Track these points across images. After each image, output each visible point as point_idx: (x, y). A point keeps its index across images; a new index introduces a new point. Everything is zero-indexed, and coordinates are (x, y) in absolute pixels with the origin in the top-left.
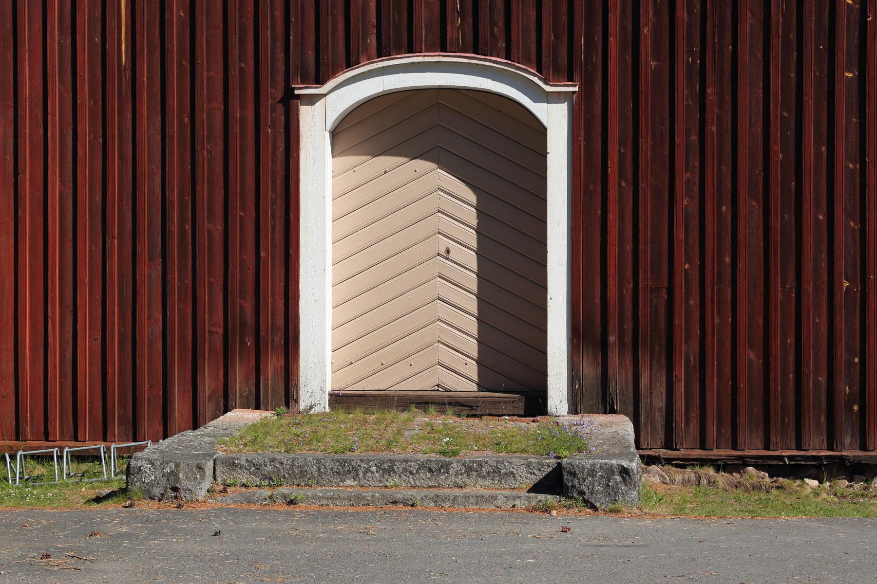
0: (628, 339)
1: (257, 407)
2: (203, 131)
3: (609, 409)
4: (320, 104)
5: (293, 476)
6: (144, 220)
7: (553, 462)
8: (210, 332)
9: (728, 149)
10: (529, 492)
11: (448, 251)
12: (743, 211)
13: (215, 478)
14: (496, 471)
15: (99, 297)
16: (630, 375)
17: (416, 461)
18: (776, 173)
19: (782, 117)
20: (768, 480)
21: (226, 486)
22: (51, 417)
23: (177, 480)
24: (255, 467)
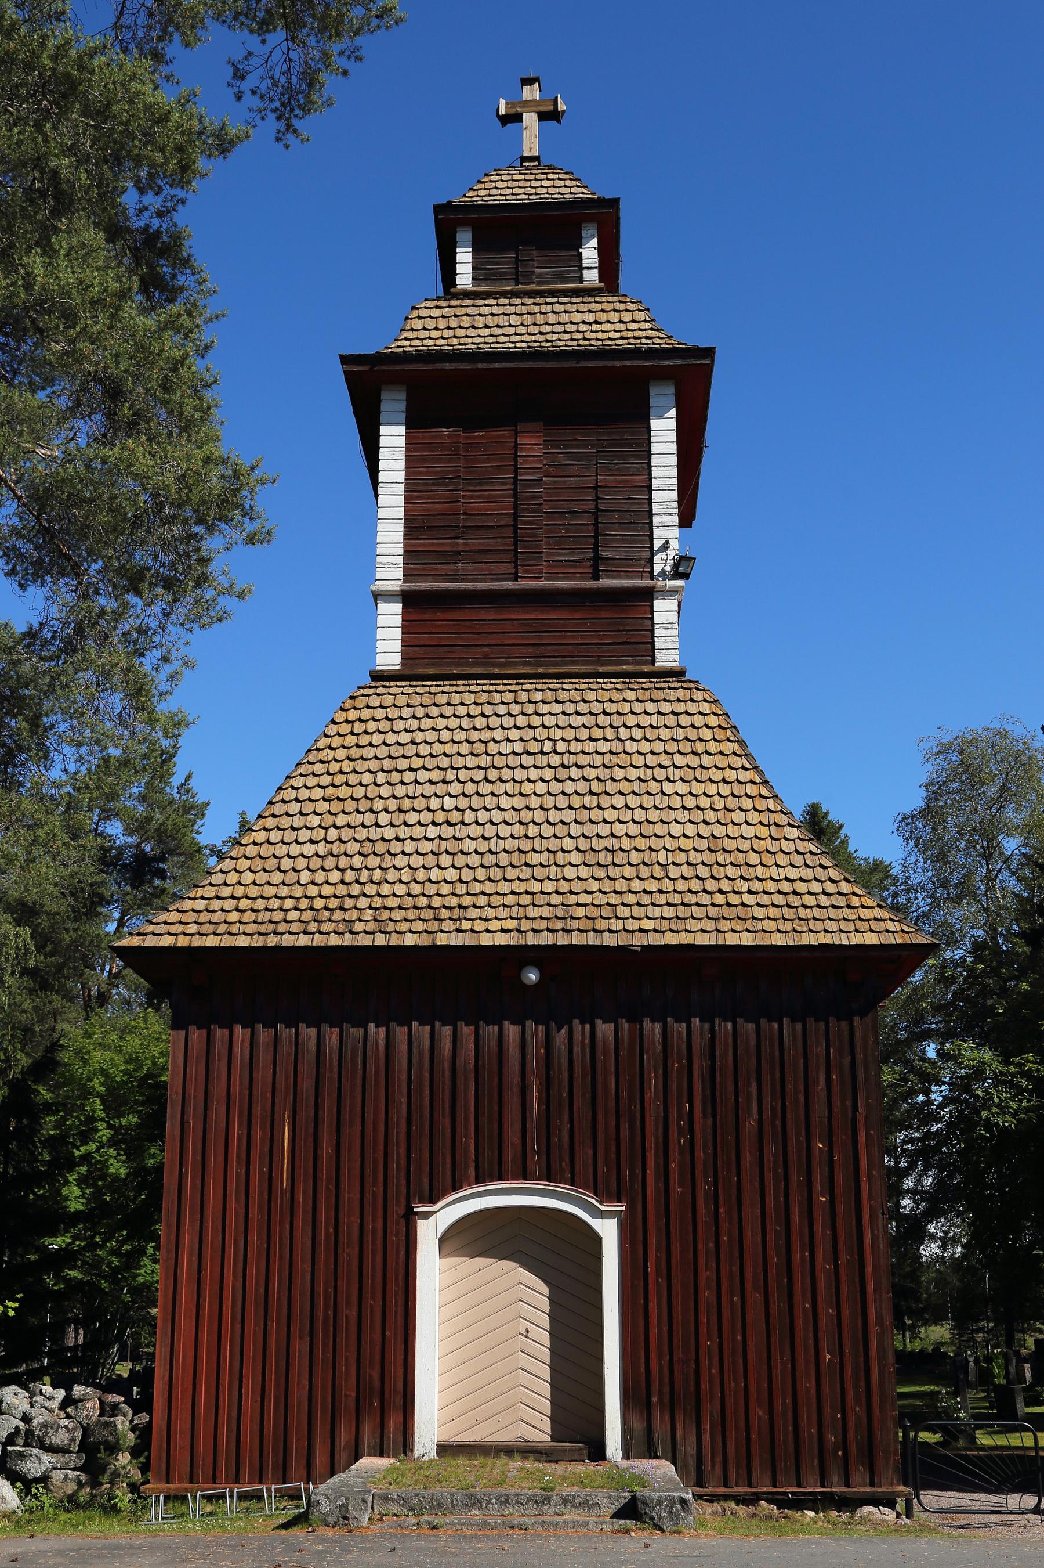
0: (666, 1400)
1: (381, 1456)
2: (344, 1239)
3: (652, 1454)
4: (432, 1218)
5: (432, 1507)
6: (297, 1308)
7: (627, 1495)
8: (346, 1395)
9: (737, 1254)
10: (612, 1518)
11: (527, 1331)
12: (749, 1301)
13: (373, 1509)
14: (586, 1502)
15: (260, 1368)
16: (669, 1428)
17: (525, 1495)
18: (773, 1272)
19: (776, 1230)
20: (776, 1511)
21: (382, 1516)
22: (218, 1465)
23: (347, 1510)
24: (404, 1501)
